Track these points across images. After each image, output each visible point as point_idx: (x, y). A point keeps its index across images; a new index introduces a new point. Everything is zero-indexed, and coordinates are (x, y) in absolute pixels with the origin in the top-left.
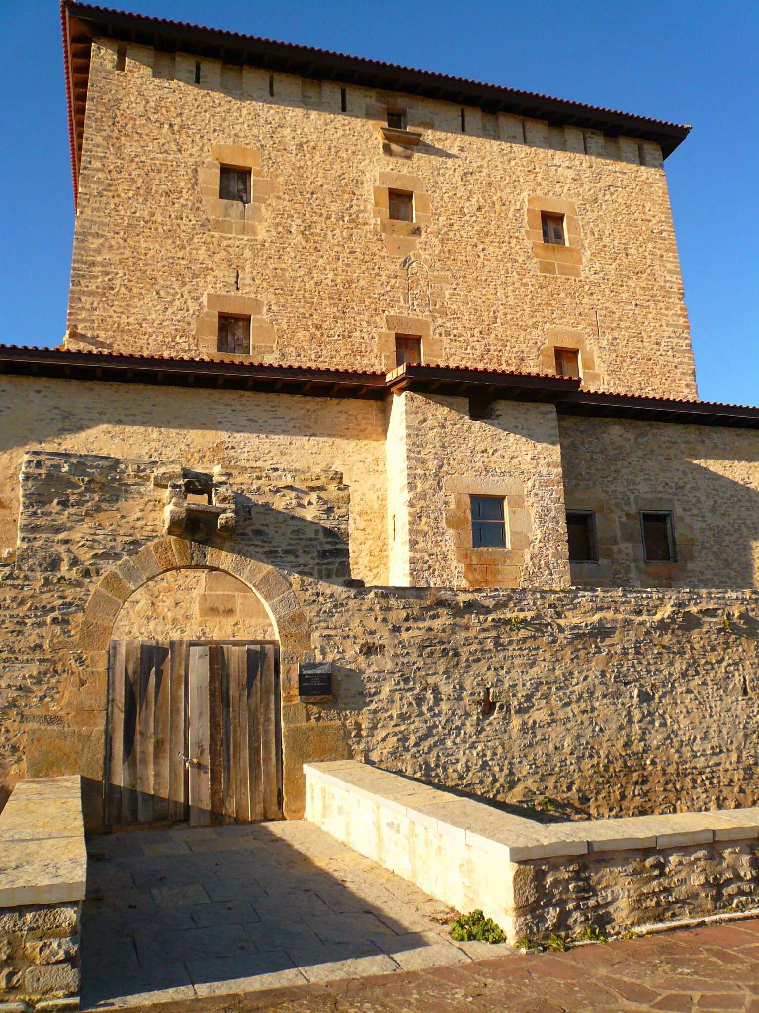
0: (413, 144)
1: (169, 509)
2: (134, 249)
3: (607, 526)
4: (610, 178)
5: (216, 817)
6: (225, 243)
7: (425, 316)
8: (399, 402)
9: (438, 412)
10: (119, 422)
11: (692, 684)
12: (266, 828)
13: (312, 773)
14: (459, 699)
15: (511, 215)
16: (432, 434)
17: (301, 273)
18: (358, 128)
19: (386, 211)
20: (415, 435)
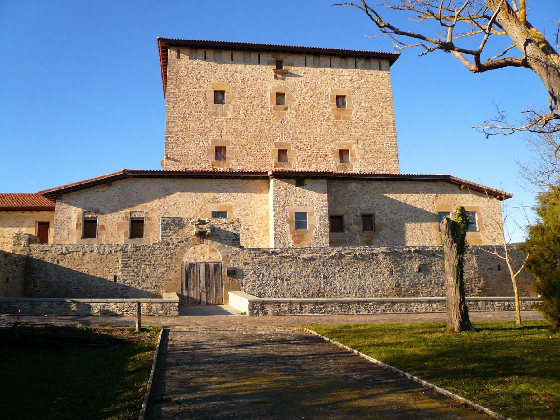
0: (286, 74)
1: (195, 230)
2: (185, 125)
3: (349, 219)
4: (366, 78)
5: (207, 304)
6: (216, 120)
7: (289, 142)
8: (272, 181)
9: (284, 185)
10: (183, 191)
11: (341, 274)
12: (221, 308)
13: (230, 293)
14: (270, 276)
15: (324, 98)
16: (282, 192)
17: (244, 129)
18: (265, 70)
19: (275, 102)
20: (276, 193)
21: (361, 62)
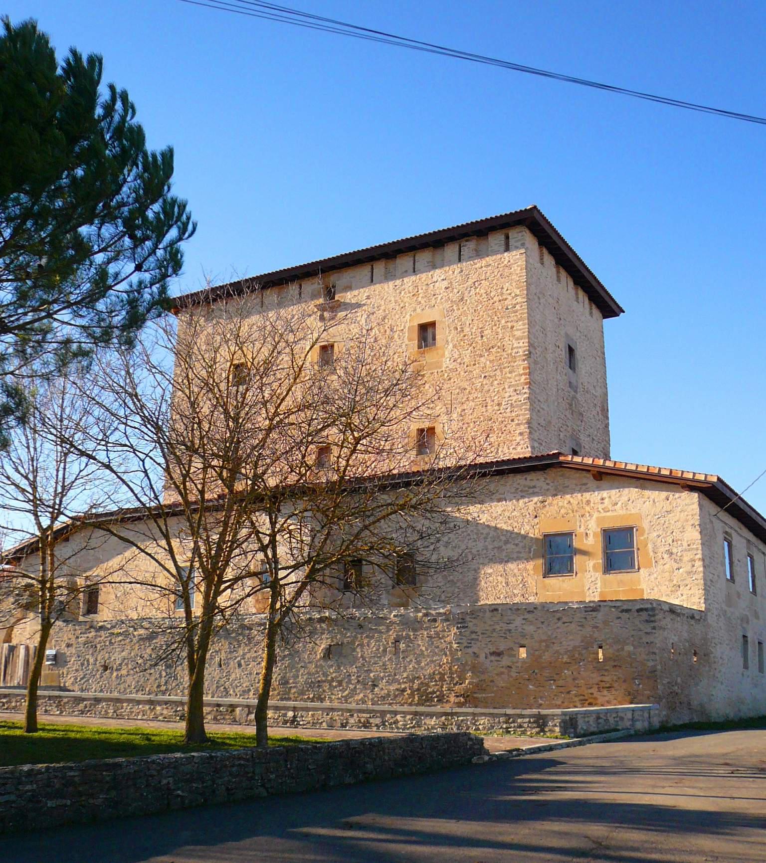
21: (469, 246)
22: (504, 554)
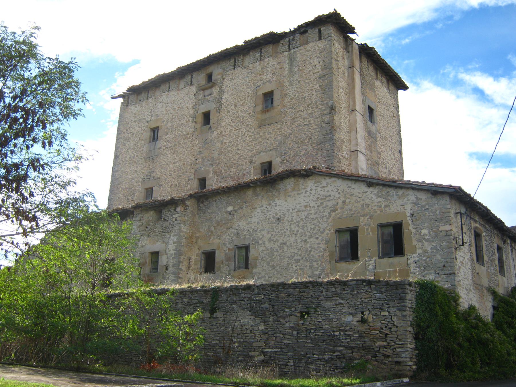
22: (309, 245)
